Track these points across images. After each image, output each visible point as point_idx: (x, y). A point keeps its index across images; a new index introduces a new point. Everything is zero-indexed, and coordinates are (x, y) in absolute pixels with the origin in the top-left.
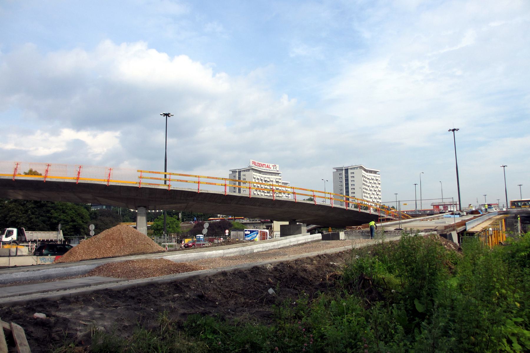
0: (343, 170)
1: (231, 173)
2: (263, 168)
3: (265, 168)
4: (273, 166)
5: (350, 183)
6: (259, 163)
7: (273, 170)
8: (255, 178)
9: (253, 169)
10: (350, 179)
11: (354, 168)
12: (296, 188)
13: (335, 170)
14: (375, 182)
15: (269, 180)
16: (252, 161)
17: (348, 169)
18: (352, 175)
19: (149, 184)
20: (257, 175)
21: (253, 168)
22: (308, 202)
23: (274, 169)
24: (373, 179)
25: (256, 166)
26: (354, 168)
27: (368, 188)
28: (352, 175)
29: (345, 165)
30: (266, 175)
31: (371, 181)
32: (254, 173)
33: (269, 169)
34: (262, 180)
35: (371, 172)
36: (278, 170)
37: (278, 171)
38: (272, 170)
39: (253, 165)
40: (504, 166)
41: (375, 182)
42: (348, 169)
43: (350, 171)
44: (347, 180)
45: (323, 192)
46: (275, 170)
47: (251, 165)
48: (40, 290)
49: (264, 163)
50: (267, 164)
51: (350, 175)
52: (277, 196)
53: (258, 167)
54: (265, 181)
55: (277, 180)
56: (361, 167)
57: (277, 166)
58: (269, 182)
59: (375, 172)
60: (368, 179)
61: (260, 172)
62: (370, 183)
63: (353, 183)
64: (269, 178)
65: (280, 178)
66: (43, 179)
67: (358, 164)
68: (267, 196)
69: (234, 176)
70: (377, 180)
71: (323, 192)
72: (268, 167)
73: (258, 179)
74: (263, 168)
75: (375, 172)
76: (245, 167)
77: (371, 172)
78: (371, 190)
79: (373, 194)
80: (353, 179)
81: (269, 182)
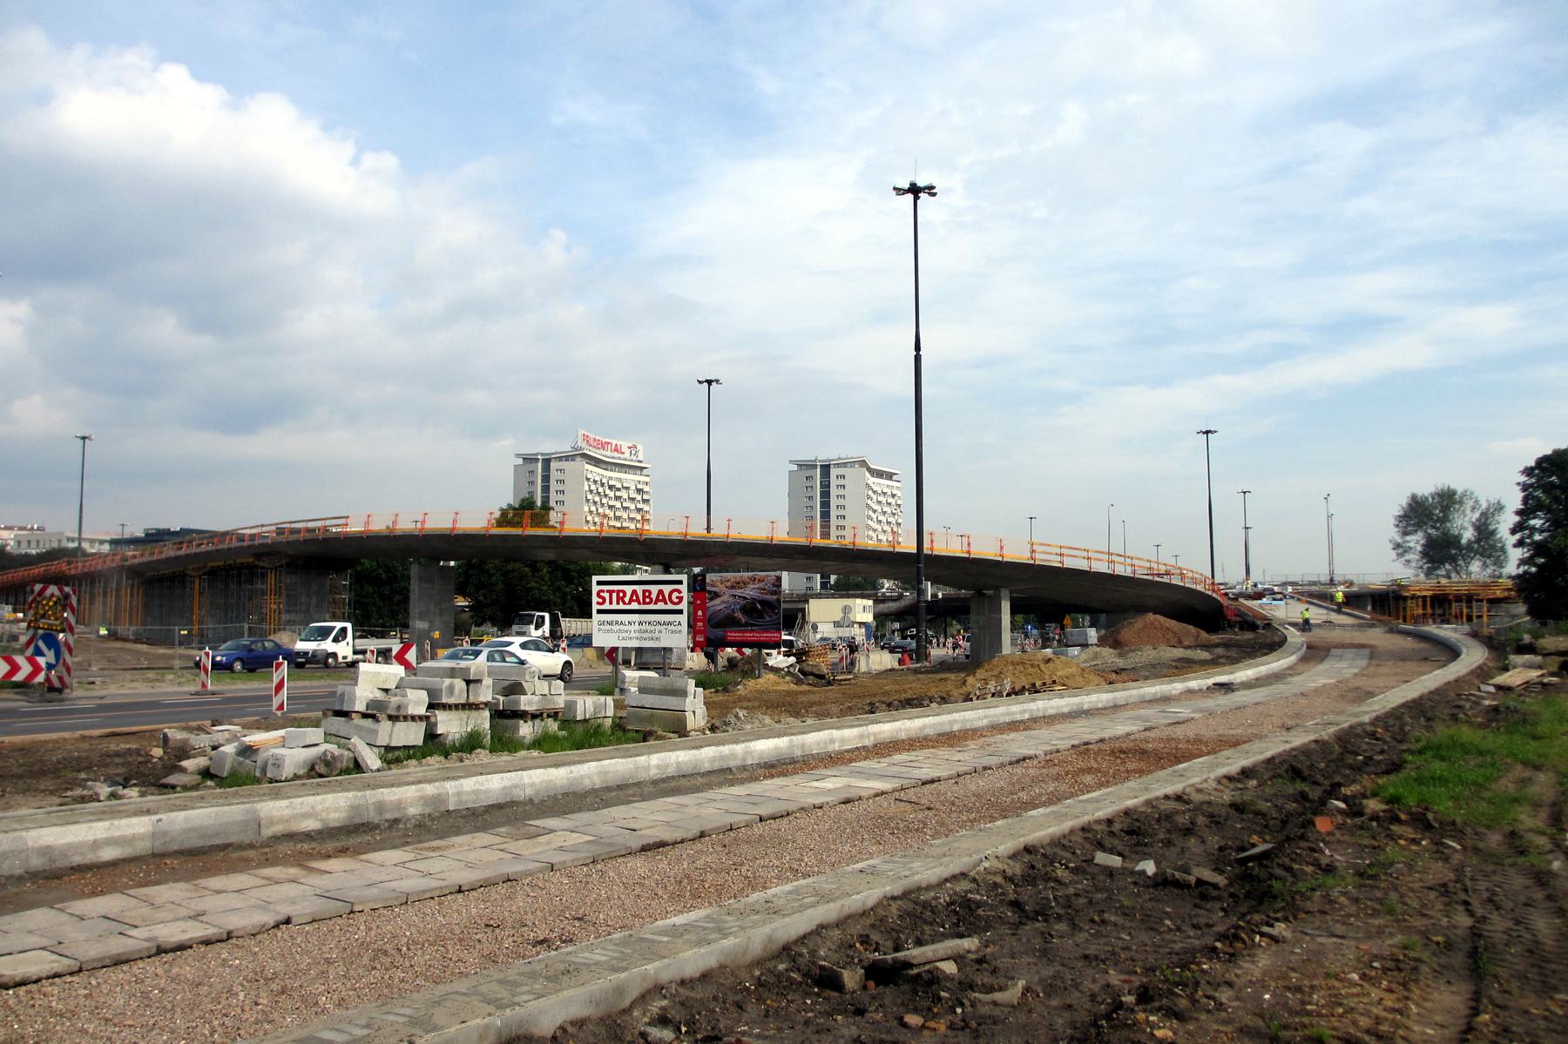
0: (815, 466)
1: (520, 461)
2: (605, 453)
3: (609, 453)
4: (629, 448)
5: (834, 502)
6: (597, 438)
7: (629, 458)
8: (588, 479)
9: (585, 456)
10: (834, 491)
11: (845, 465)
12: (1064, 547)
13: (795, 468)
14: (890, 500)
15: (619, 486)
16: (583, 432)
17: (829, 466)
18: (841, 482)
19: (1045, 560)
20: (595, 472)
21: (586, 452)
22: (1145, 577)
23: (632, 457)
24: (885, 494)
25: (590, 445)
26: (845, 465)
27: (874, 516)
28: (841, 482)
29: (823, 455)
30: (611, 470)
31: (880, 499)
32: (588, 467)
33: (619, 455)
34: (603, 485)
35: (879, 474)
36: (640, 458)
37: (640, 462)
38: (626, 458)
39: (584, 445)
40: (1245, 493)
41: (890, 500)
42: (829, 466)
43: (834, 472)
44: (826, 494)
45: (1120, 556)
46: (634, 458)
47: (581, 444)
48: (318, 875)
49: (607, 440)
50: (614, 442)
51: (834, 481)
52: (610, 527)
53: (594, 450)
54: (611, 487)
55: (639, 487)
56: (863, 463)
57: (640, 447)
58: (619, 490)
59: (890, 476)
60: (875, 492)
61: (597, 462)
62: (879, 502)
63: (841, 502)
64: (620, 480)
65: (647, 479)
66: (557, 534)
67: (853, 453)
68: (614, 527)
69: (532, 472)
70: (893, 496)
71: (1120, 556)
72: (616, 450)
73: (595, 482)
74: (605, 453)
75: (890, 476)
76: (566, 448)
77: (879, 474)
78: (880, 522)
79: (885, 532)
80: (841, 492)
81: (619, 490)
